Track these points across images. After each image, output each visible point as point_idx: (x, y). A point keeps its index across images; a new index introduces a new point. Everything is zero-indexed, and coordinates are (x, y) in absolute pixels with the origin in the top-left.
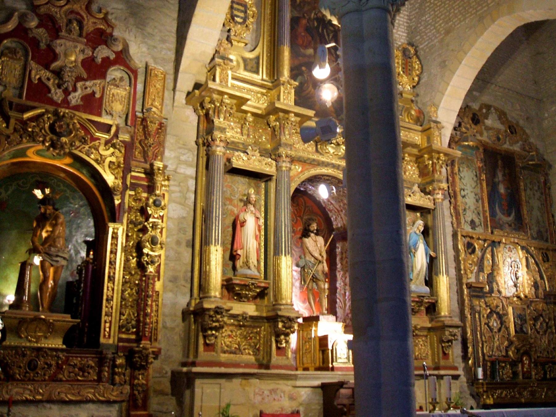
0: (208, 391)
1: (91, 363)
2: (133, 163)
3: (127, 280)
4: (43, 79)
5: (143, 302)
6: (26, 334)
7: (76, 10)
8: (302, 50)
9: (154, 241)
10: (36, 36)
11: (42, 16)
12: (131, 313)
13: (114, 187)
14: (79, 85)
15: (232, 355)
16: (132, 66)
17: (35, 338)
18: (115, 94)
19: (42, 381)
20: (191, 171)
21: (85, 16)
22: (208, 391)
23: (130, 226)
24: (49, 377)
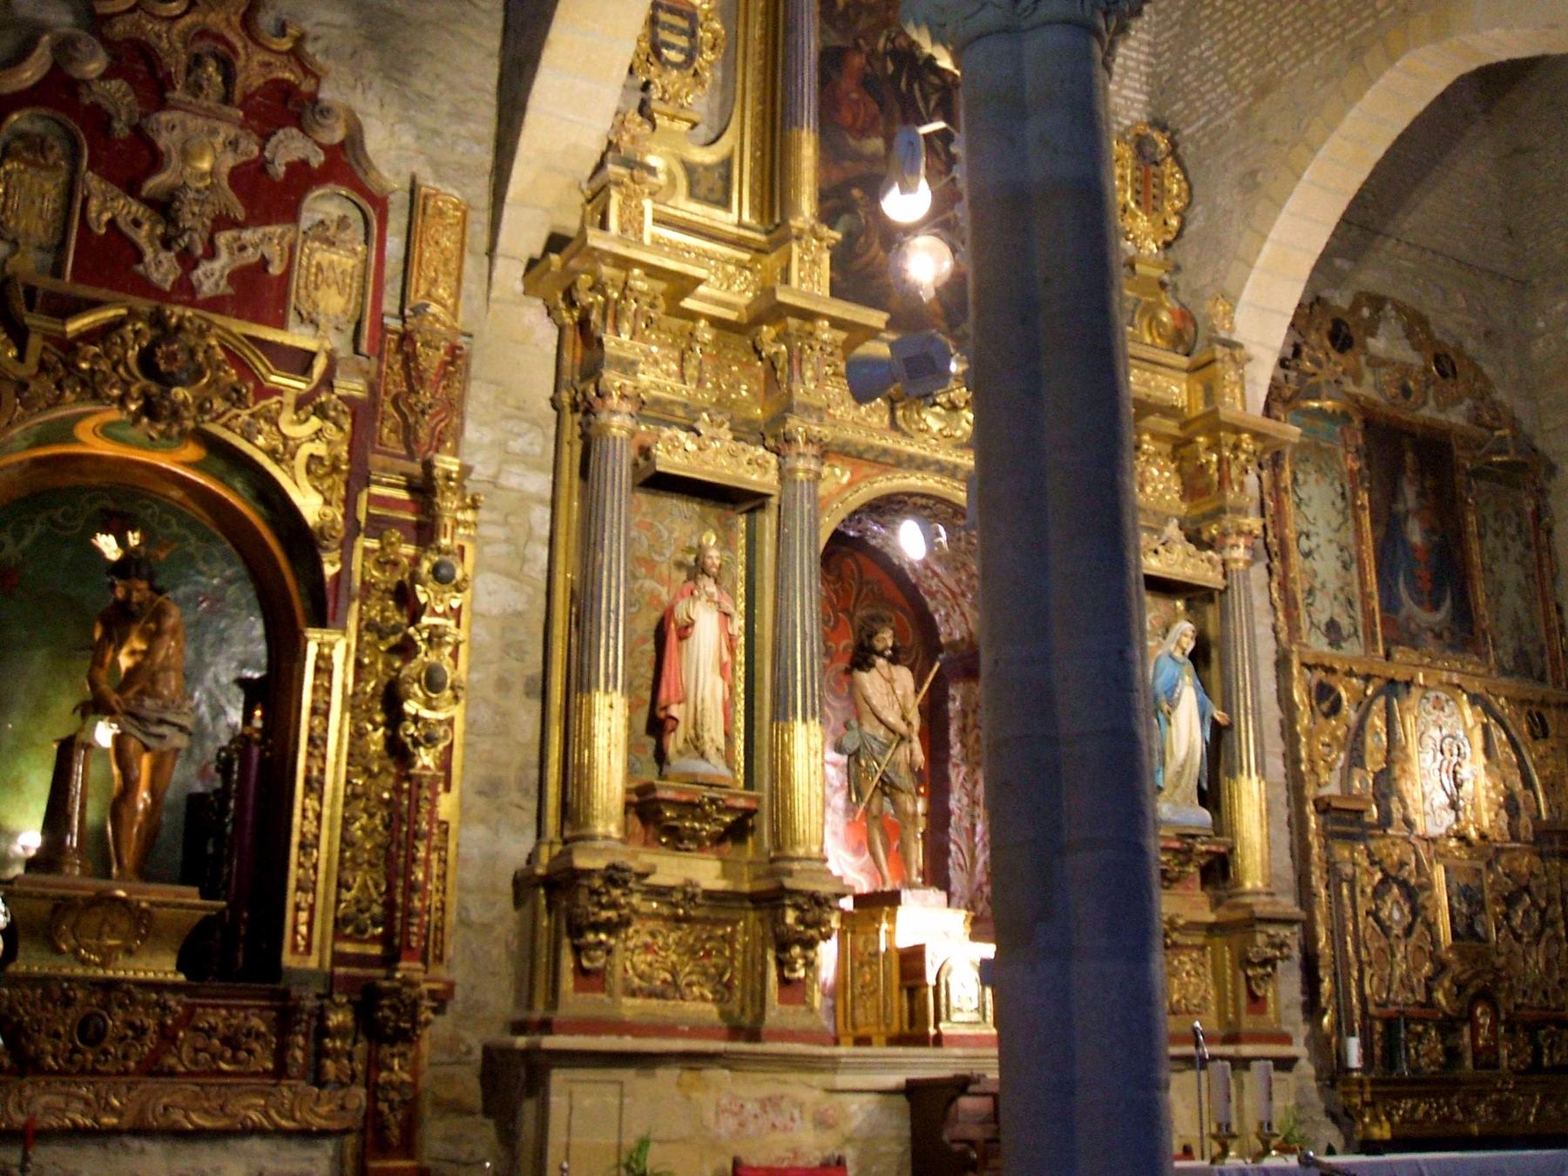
0: (587, 1102)
1: (257, 1023)
2: (376, 460)
3: (359, 790)
4: (121, 222)
5: (402, 853)
6: (73, 942)
7: (214, 29)
8: (851, 141)
9: (433, 681)
10: (101, 100)
11: (119, 44)
12: (370, 883)
13: (322, 529)
14: (223, 238)
15: (654, 1002)
16: (373, 187)
17: (98, 952)
18: (325, 264)
19: (119, 1073)
20: (540, 483)
21: (239, 45)
22: (587, 1102)
23: (367, 637)
24: (138, 1063)
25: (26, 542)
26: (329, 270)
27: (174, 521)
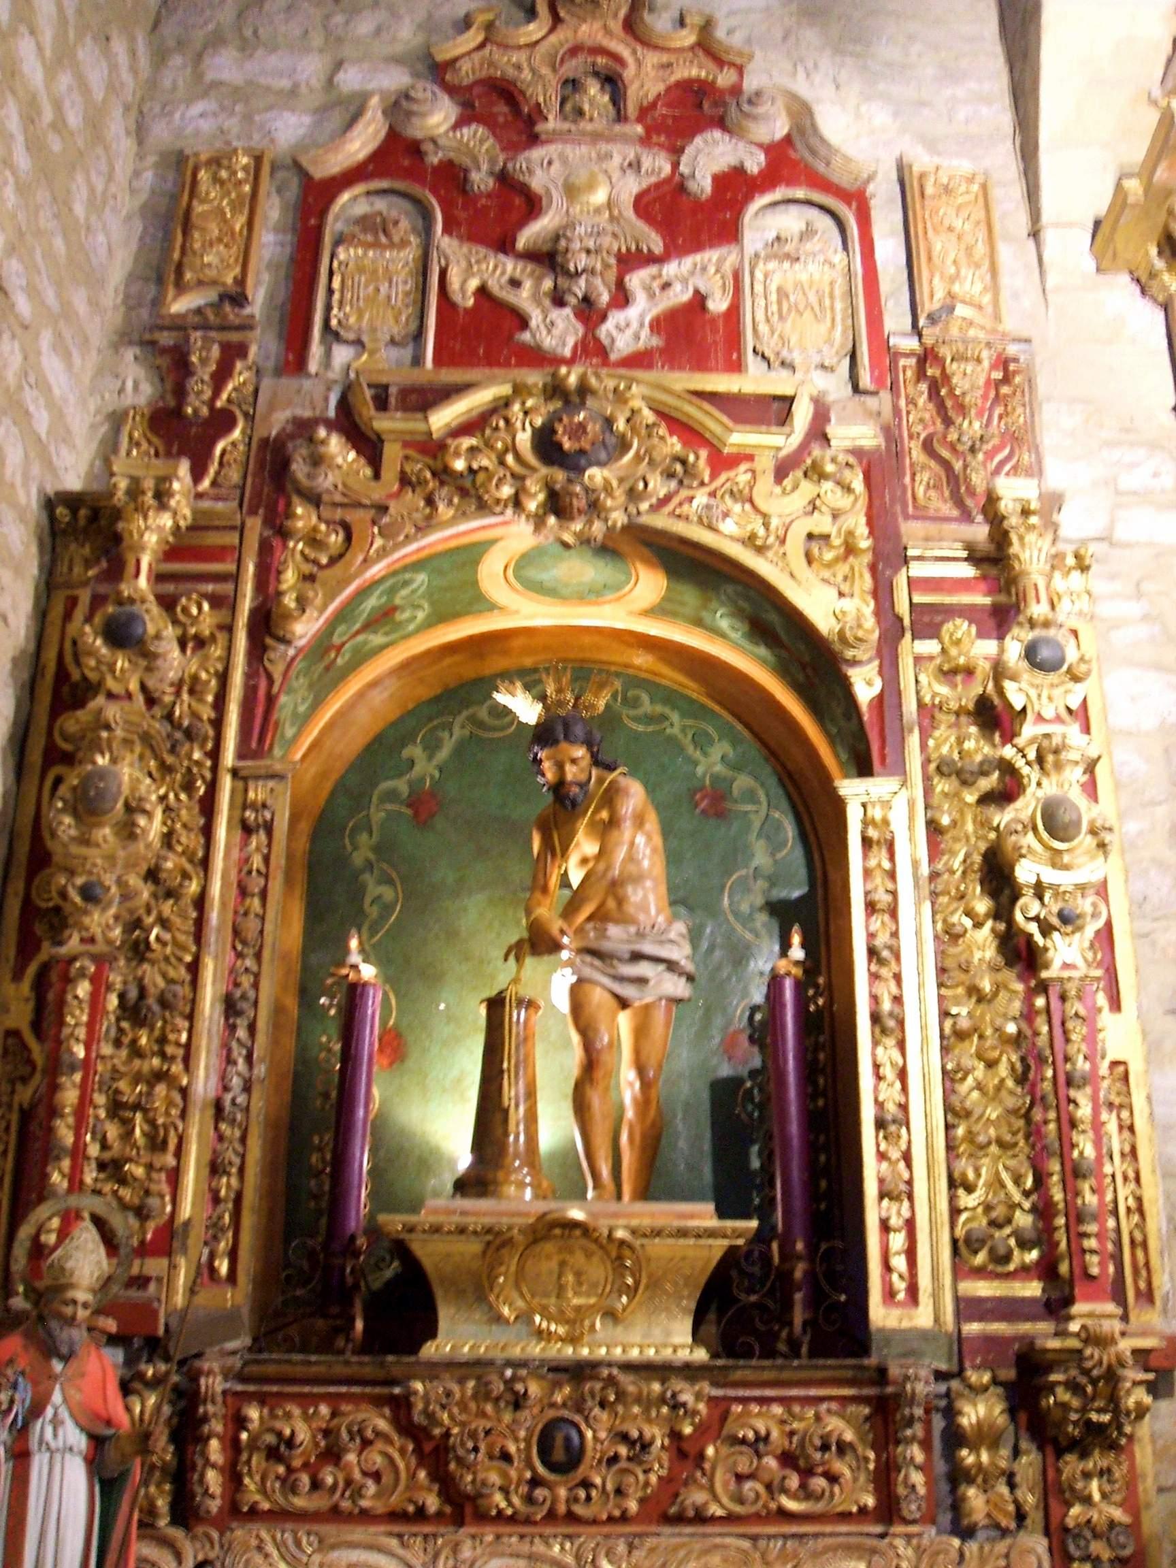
1: (840, 1427)
2: (911, 530)
3: (964, 1024)
4: (494, 287)
5: (1052, 1115)
6: (520, 1303)
7: (589, 43)
9: (1055, 822)
10: (452, 155)
11: (470, 88)
12: (1006, 1177)
13: (841, 634)
14: (636, 280)
16: (843, 179)
17: (561, 1318)
18: (789, 288)
19: (611, 1519)
21: (626, 53)
23: (942, 785)
24: (642, 1501)
25: (443, 754)
26: (786, 272)
27: (645, 698)
